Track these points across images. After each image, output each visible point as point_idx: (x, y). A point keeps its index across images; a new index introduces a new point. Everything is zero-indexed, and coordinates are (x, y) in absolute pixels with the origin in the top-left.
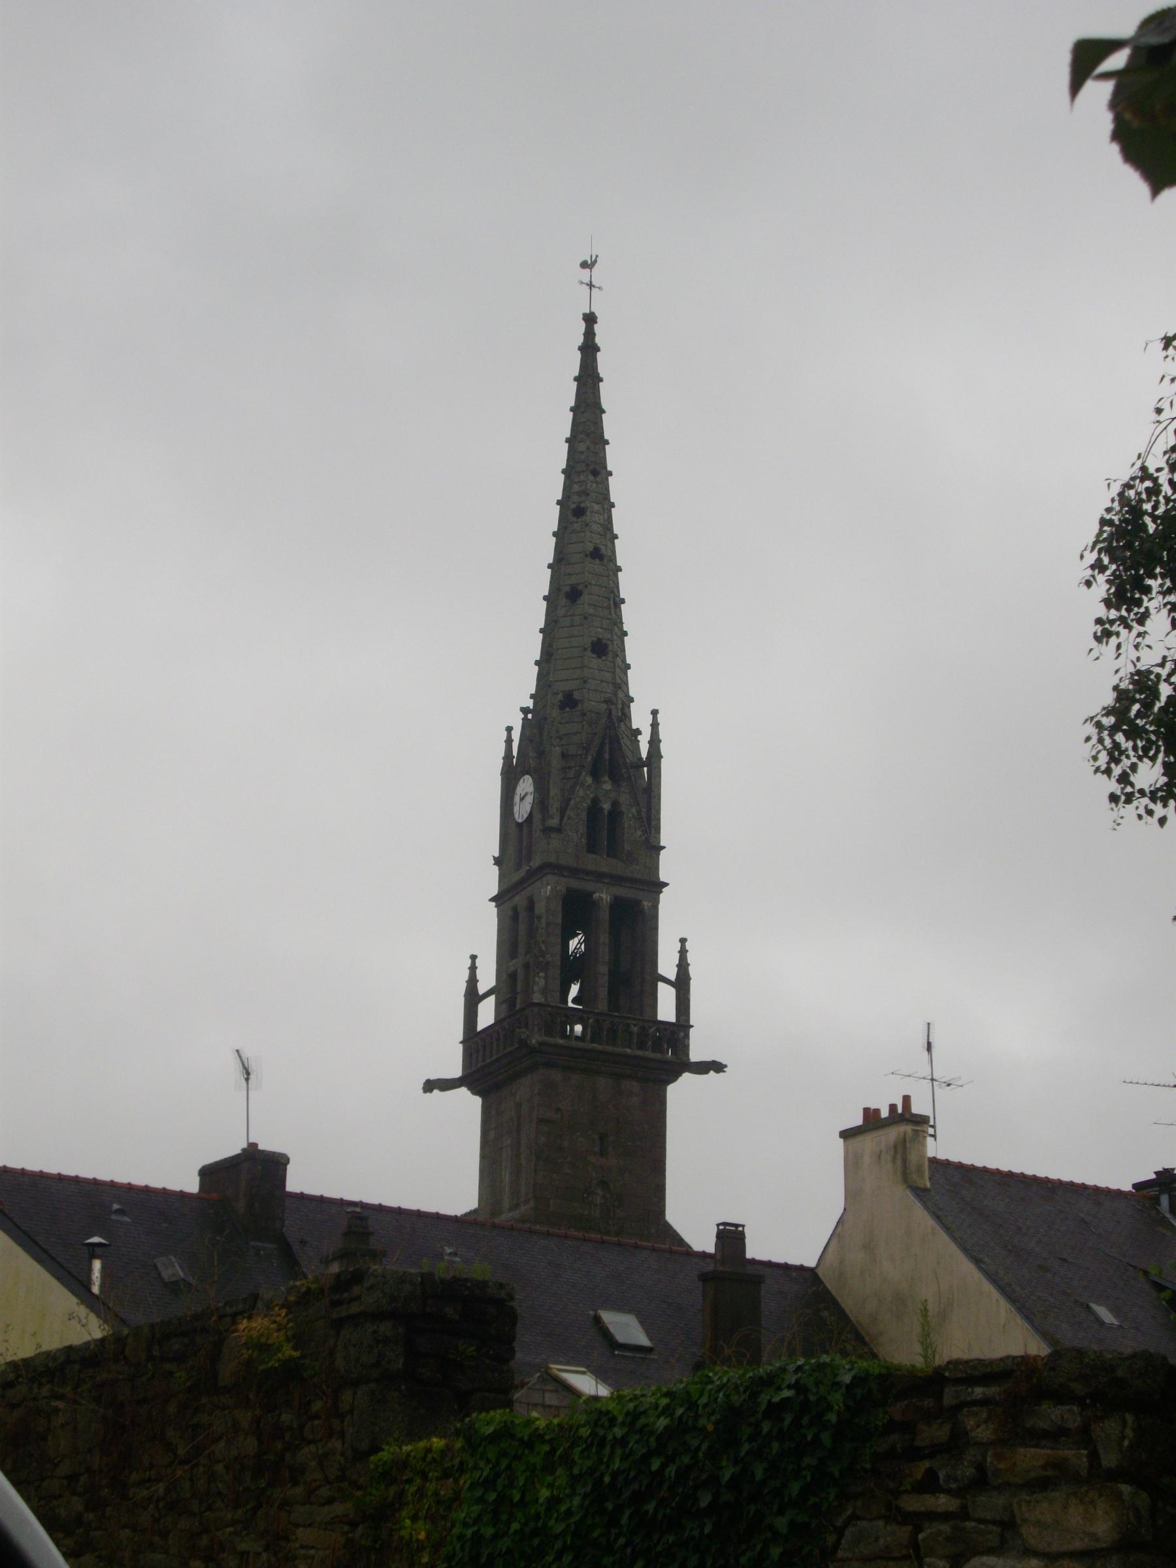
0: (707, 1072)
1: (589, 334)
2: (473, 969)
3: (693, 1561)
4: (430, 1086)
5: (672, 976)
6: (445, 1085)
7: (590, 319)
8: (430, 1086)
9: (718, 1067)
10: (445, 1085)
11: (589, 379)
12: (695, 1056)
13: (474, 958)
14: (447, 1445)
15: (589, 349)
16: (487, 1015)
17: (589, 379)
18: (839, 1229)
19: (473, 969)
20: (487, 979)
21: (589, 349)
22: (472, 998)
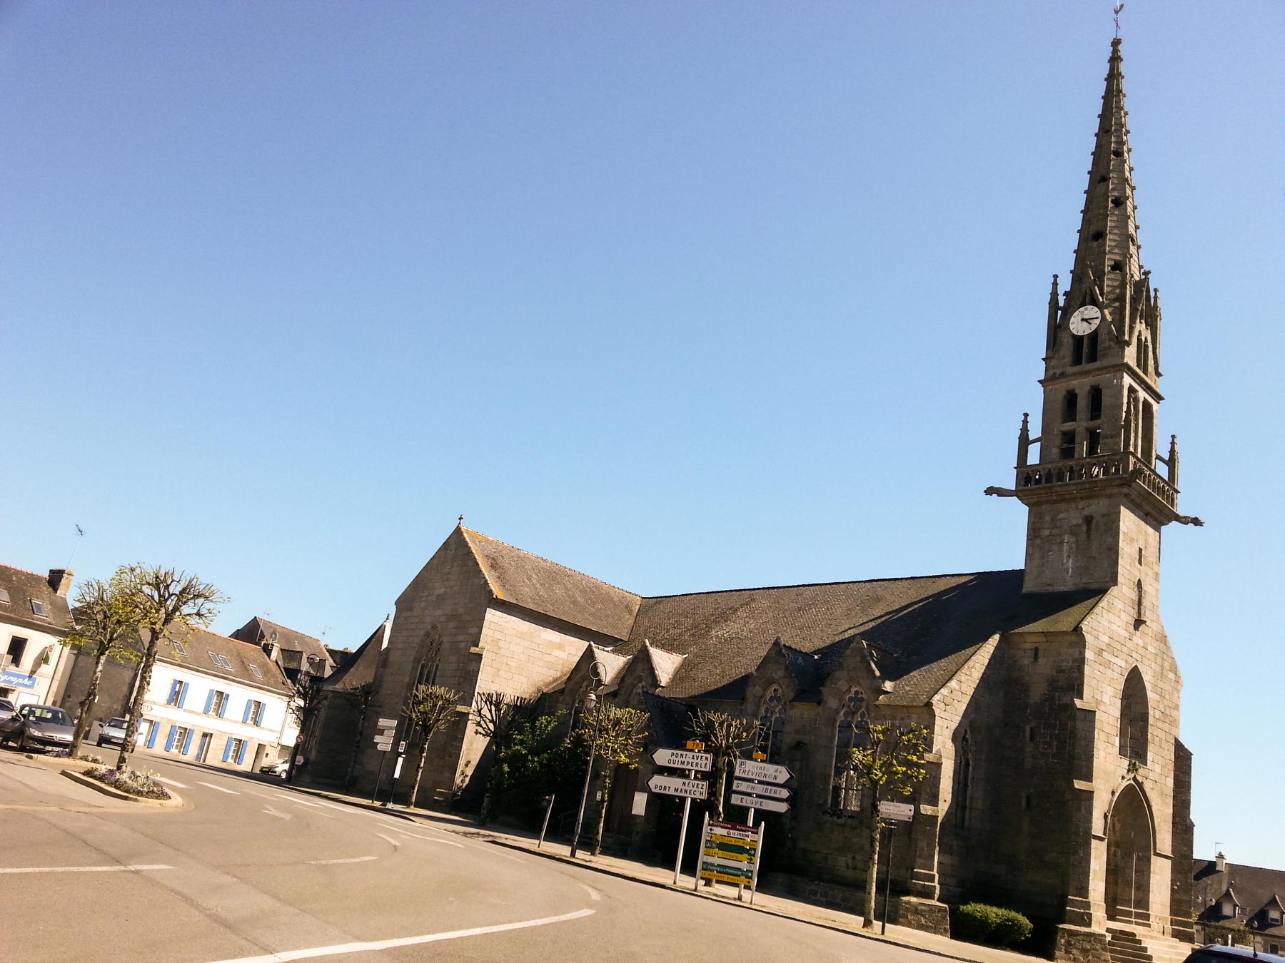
0: (1186, 523)
1: (1115, 51)
2: (1025, 422)
3: (35, 691)
4: (990, 491)
5: (1166, 457)
6: (1001, 492)
7: (1116, 43)
8: (990, 491)
9: (1196, 522)
10: (1001, 492)
11: (1114, 77)
12: (1182, 508)
13: (1026, 415)
14: (599, 682)
15: (1115, 59)
16: (1034, 456)
17: (1114, 77)
18: (855, 586)
19: (1025, 422)
20: (1035, 431)
21: (1115, 59)
22: (1024, 442)
